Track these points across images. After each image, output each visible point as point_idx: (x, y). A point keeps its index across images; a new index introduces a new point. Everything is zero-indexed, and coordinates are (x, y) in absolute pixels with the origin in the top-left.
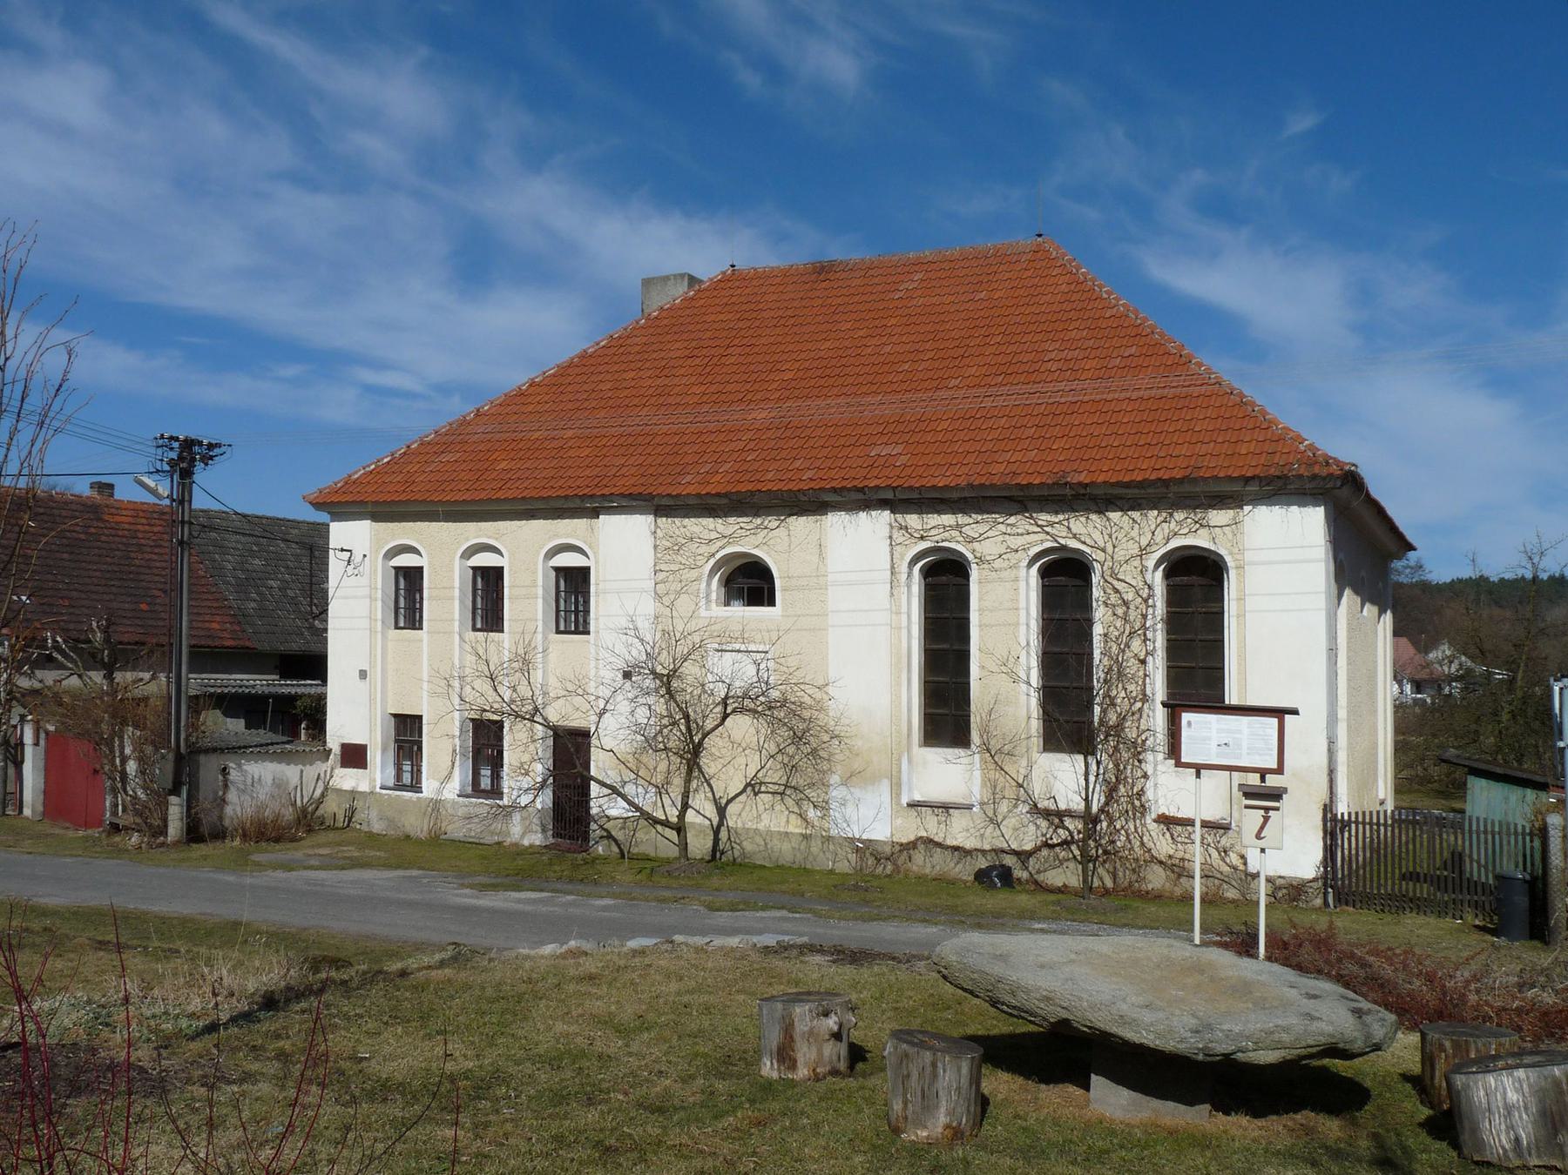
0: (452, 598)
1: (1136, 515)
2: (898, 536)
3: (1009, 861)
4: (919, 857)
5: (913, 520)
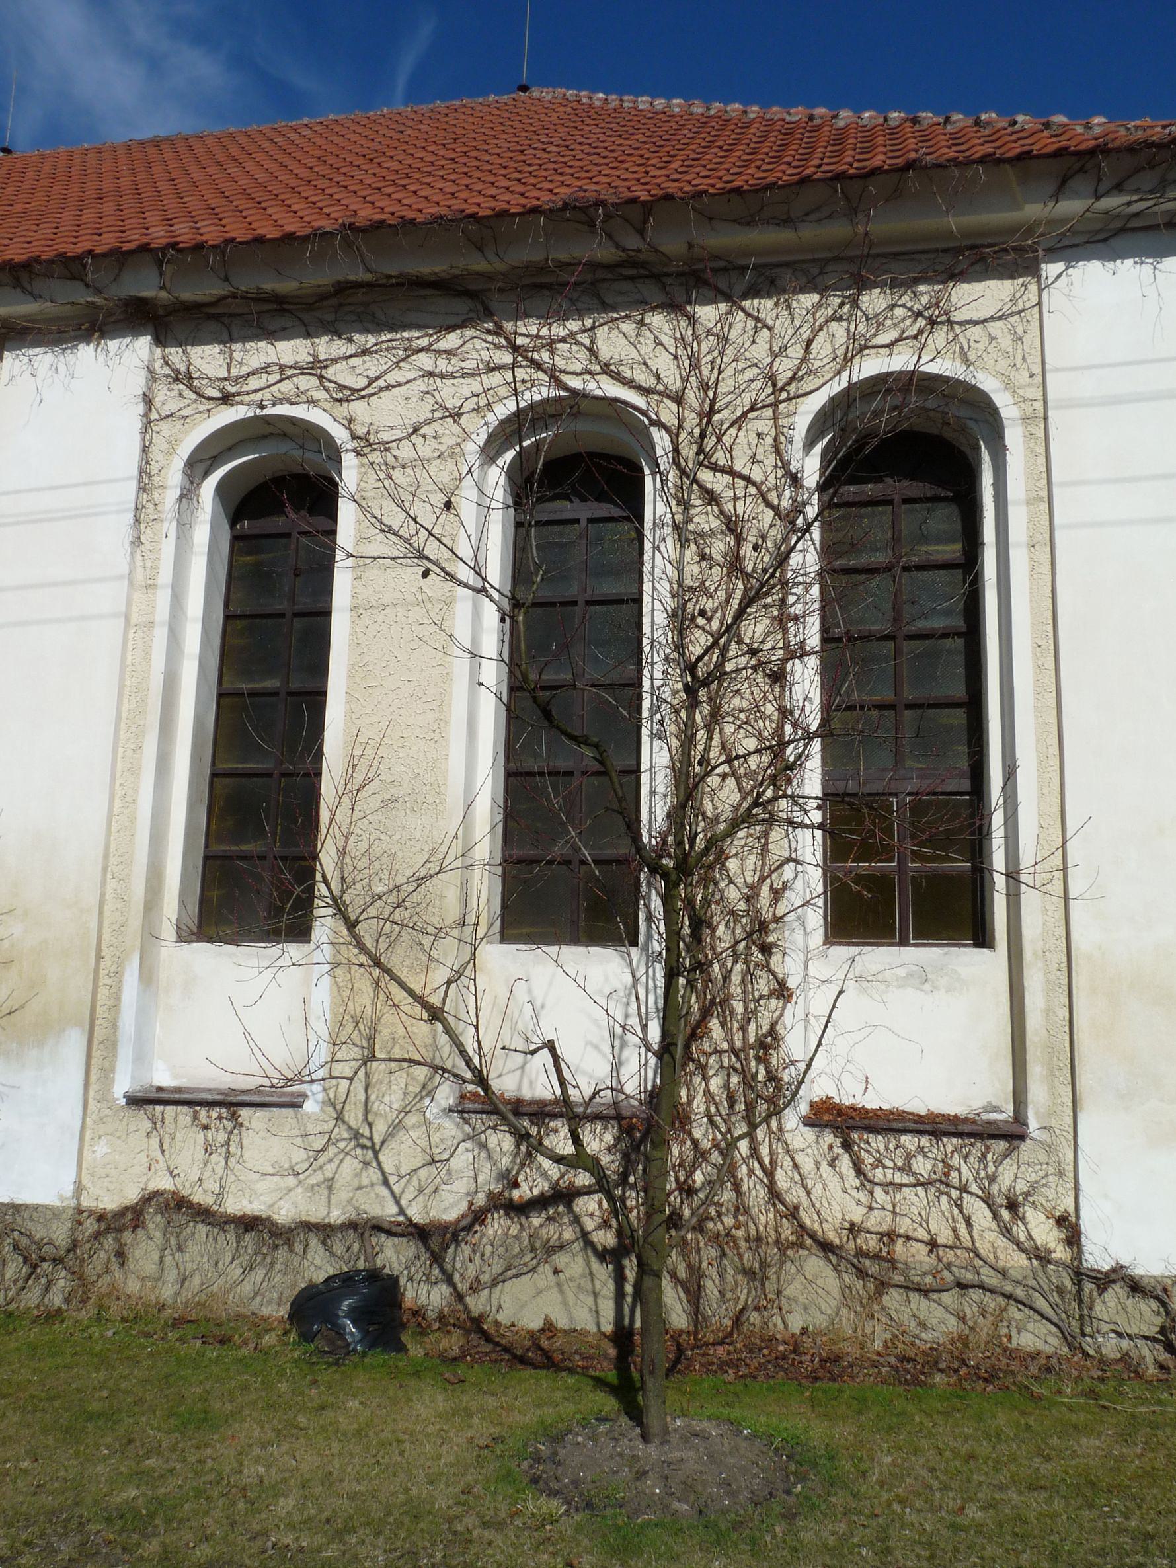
1: (765, 307)
2: (168, 398)
3: (394, 1256)
4: (145, 1251)
5: (208, 359)
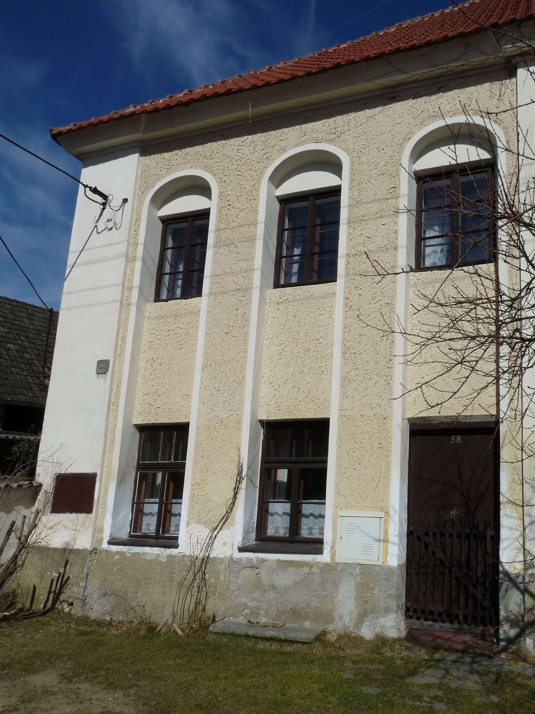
0: (252, 239)
